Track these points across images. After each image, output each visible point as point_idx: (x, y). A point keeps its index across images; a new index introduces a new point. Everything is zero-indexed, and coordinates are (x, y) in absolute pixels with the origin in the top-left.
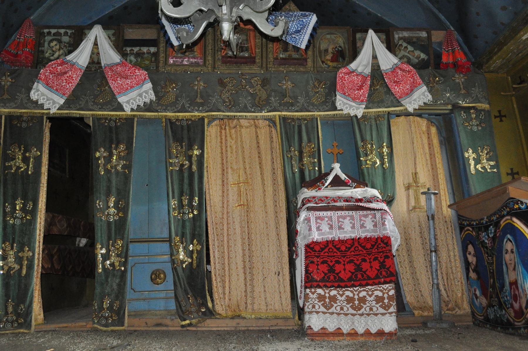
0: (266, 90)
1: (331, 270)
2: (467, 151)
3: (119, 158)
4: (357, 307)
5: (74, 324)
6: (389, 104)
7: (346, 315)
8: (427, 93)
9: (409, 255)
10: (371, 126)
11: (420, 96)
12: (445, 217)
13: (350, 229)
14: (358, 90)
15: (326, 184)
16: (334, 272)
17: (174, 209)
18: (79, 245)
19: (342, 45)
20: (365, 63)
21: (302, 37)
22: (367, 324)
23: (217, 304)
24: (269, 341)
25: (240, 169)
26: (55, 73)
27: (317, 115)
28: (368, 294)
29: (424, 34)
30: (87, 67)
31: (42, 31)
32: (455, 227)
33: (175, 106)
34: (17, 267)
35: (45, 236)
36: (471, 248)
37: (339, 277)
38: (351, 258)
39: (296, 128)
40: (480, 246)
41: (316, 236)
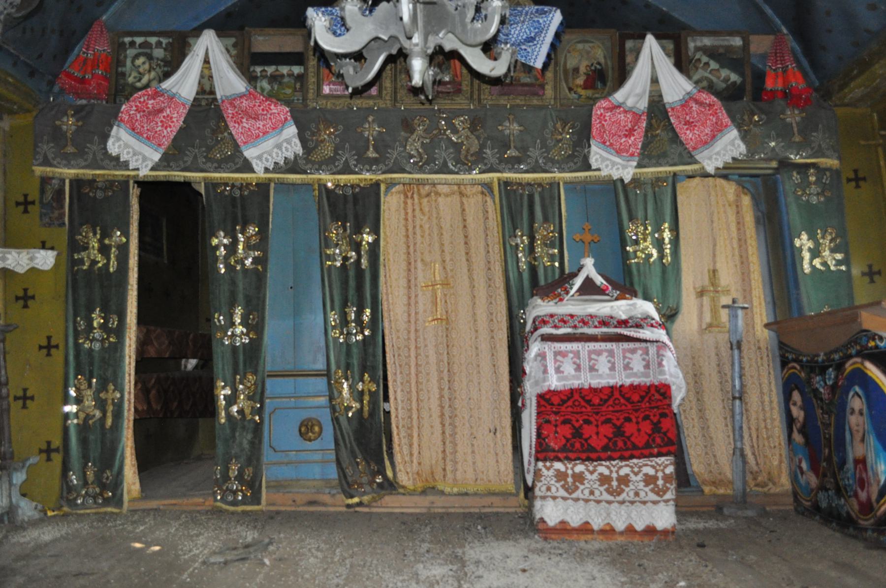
0: (478, 138)
1: (577, 433)
2: (799, 237)
3: (248, 247)
4: (615, 491)
5: (186, 501)
6: (676, 160)
7: (598, 502)
8: (739, 142)
9: (698, 400)
10: (645, 196)
11: (729, 146)
12: (758, 341)
13: (607, 371)
14: (626, 136)
15: (572, 292)
16: (581, 437)
17: (334, 327)
18: (186, 367)
19: (602, 61)
20: (638, 90)
21: (537, 49)
22: (629, 516)
23: (400, 470)
24: (479, 537)
25: (435, 262)
26: (144, 111)
27: (560, 179)
28: (633, 472)
29: (737, 42)
30: (195, 99)
31: (121, 40)
32: (773, 357)
33: (334, 164)
34: (98, 414)
35: (137, 362)
36: (796, 396)
37: (589, 445)
38: (609, 416)
39: (526, 198)
40: (811, 398)
41: (554, 383)
